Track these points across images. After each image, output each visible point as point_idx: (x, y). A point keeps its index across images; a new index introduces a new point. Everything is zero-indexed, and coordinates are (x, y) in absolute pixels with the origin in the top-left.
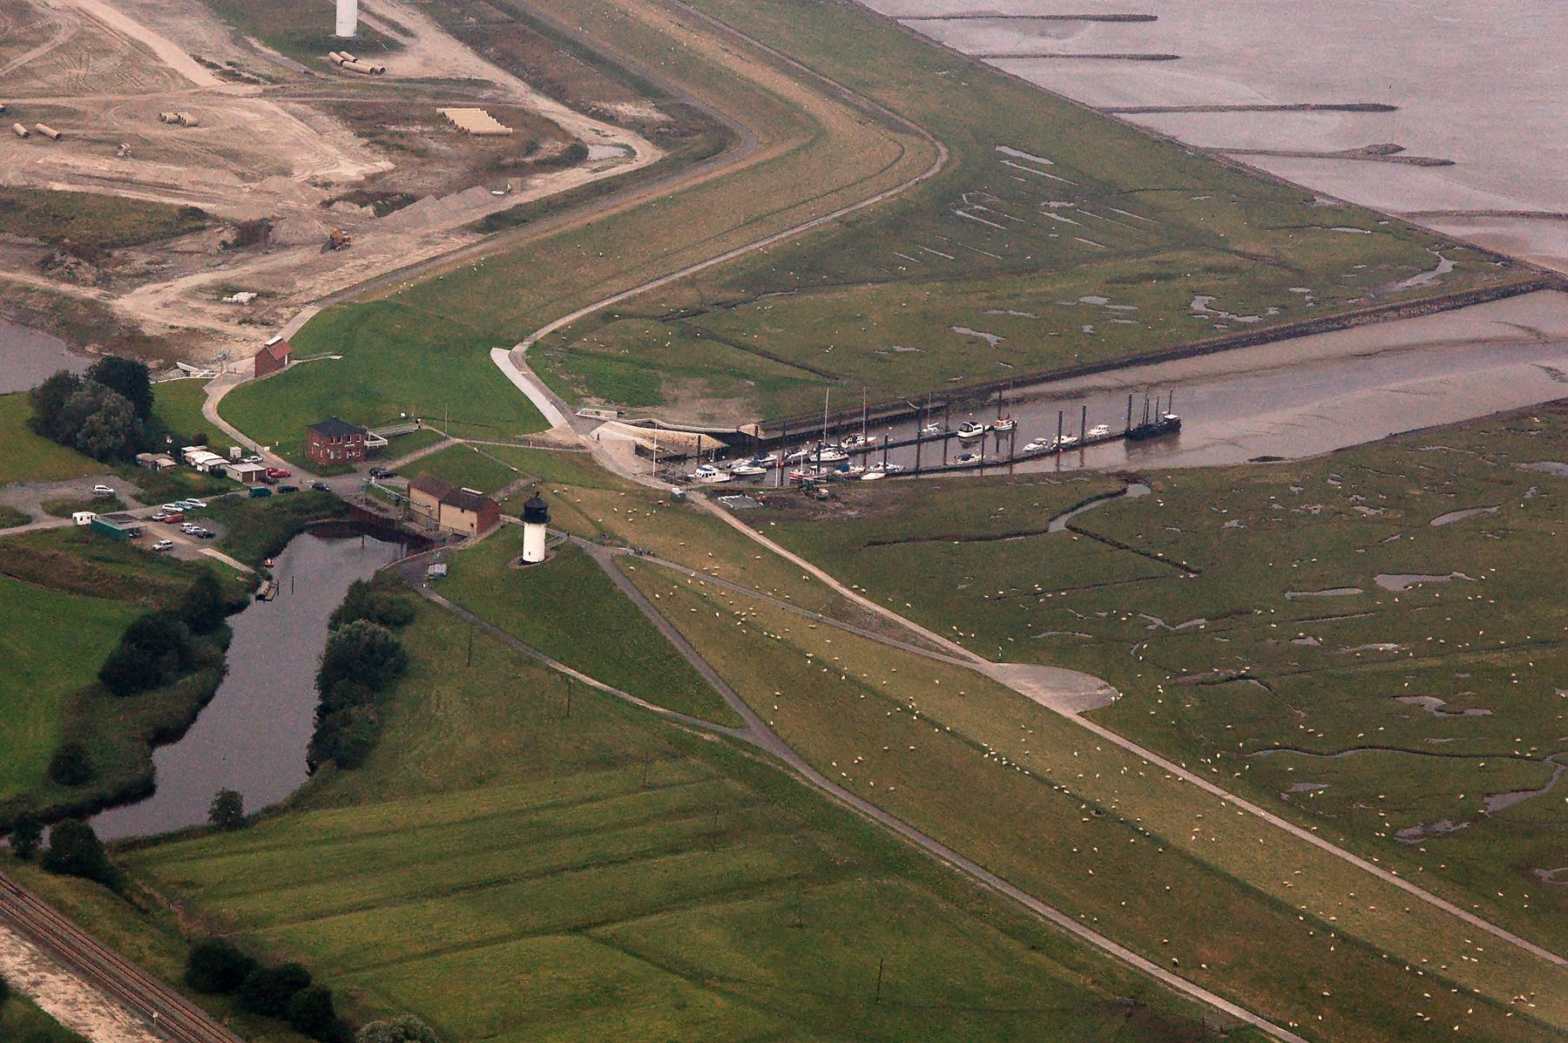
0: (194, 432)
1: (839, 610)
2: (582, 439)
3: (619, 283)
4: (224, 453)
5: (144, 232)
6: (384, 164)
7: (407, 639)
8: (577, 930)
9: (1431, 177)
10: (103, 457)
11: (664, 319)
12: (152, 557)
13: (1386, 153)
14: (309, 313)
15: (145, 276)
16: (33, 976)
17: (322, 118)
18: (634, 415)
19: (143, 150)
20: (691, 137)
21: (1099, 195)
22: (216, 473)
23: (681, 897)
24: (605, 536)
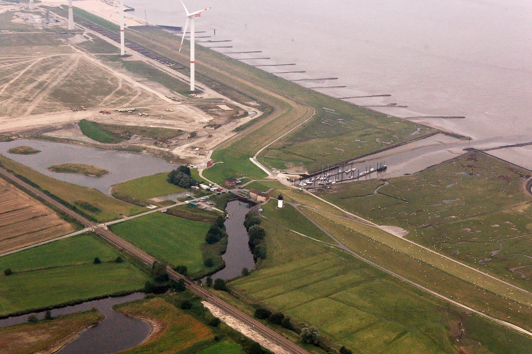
0: (201, 181)
1: (346, 216)
2: (276, 178)
3: (267, 142)
4: (208, 185)
5: (172, 135)
6: (212, 118)
7: (261, 226)
8: (327, 296)
9: (404, 110)
10: (185, 188)
11: (279, 149)
12: (203, 210)
13: (394, 105)
14: (211, 152)
15: (176, 145)
16: (223, 317)
17: (195, 108)
18: (283, 171)
19: (165, 117)
20: (267, 109)
21: (347, 117)
22: (208, 190)
23: (344, 287)
24: (293, 201)
